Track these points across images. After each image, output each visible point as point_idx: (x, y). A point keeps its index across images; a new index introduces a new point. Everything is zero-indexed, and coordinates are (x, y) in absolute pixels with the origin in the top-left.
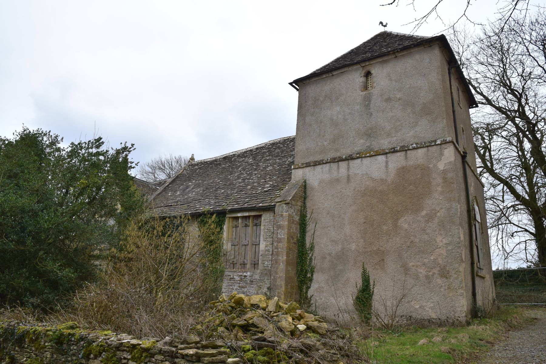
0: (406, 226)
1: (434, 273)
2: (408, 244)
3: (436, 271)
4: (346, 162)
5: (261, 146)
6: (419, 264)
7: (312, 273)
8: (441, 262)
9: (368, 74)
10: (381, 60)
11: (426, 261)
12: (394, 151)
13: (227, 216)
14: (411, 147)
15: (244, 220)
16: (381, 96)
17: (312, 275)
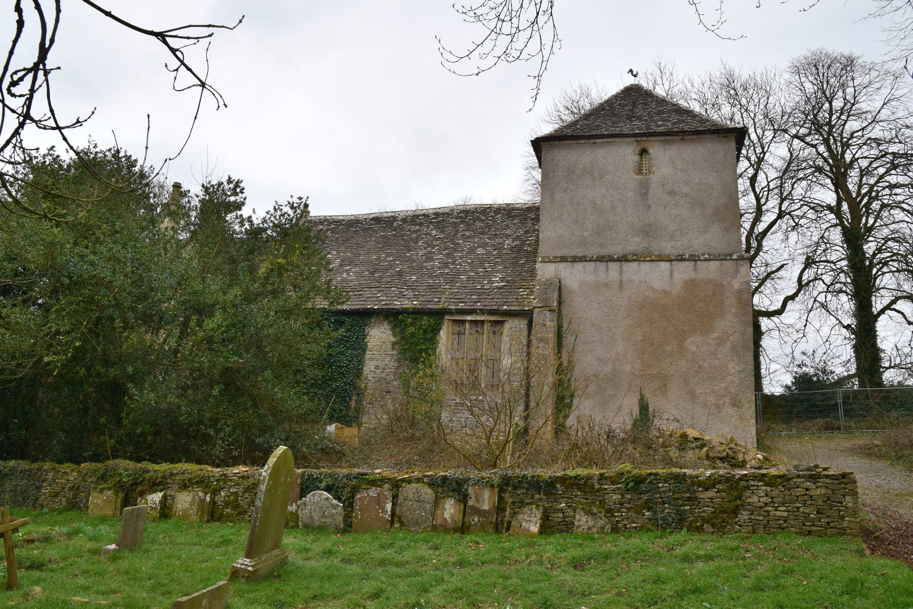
0: (694, 348)
1: (725, 402)
2: (696, 369)
3: (727, 399)
4: (619, 263)
5: (442, 210)
6: (709, 391)
7: (572, 396)
9: (643, 152)
10: (663, 138)
11: (716, 388)
12: (680, 258)
13: (446, 317)
14: (702, 258)
16: (663, 186)
17: (572, 401)
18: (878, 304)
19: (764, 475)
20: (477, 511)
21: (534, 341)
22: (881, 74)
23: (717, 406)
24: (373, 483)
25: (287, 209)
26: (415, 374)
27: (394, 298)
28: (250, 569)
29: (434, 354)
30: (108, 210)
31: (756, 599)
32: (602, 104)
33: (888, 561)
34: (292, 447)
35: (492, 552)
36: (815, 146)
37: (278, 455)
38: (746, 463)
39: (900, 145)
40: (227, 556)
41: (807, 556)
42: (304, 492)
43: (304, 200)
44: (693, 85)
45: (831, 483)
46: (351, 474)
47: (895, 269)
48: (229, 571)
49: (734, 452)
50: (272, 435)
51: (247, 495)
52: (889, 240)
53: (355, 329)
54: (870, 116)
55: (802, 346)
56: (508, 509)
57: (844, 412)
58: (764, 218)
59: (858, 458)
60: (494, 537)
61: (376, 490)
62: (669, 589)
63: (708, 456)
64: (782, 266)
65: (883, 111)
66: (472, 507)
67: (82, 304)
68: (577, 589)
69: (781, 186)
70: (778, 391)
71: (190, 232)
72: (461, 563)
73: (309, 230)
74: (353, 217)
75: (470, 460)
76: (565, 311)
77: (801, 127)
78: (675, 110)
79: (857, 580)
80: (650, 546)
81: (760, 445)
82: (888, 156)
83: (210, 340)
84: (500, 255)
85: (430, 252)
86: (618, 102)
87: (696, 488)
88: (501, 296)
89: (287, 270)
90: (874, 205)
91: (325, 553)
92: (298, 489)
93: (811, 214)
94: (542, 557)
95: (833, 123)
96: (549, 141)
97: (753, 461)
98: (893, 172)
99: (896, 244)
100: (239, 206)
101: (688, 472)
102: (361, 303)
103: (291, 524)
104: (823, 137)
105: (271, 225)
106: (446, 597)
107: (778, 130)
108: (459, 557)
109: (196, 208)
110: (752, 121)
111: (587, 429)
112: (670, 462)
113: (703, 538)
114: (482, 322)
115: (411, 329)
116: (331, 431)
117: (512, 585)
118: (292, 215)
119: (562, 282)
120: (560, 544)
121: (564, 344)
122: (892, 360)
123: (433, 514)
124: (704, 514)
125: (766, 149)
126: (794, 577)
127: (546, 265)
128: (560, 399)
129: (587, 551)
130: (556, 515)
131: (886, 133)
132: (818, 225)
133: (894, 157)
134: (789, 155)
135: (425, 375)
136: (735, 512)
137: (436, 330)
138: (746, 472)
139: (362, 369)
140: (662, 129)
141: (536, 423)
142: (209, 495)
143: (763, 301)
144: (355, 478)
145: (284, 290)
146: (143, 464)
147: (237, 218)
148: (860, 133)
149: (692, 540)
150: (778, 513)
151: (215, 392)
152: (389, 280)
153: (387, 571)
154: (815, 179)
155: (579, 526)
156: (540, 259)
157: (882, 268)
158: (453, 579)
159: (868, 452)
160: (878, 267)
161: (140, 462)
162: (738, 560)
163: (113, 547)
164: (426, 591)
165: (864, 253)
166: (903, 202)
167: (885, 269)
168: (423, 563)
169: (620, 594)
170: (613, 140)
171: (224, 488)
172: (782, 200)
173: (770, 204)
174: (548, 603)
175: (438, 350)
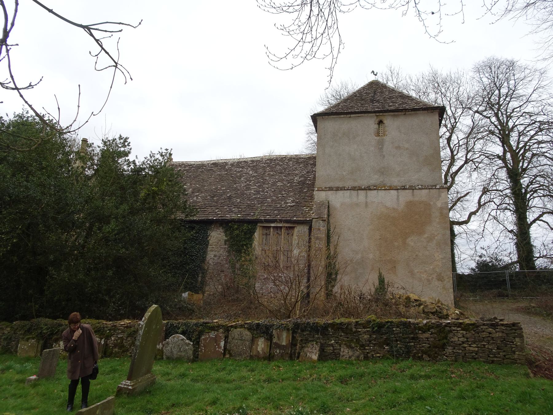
0: (412, 244)
1: (433, 278)
2: (414, 257)
3: (434, 276)
4: (365, 191)
7: (336, 274)
8: (438, 270)
9: (380, 122)
12: (404, 188)
13: (258, 225)
14: (417, 188)
15: (287, 230)
16: (392, 143)
17: (336, 277)
18: (530, 217)
19: (461, 323)
20: (278, 346)
21: (313, 239)
22: (532, 71)
23: (428, 280)
24: (213, 329)
25: (158, 156)
26: (239, 260)
27: (226, 213)
28: (130, 387)
29: (251, 247)
30: (37, 154)
31: (460, 404)
32: (355, 93)
33: (546, 381)
34: (161, 306)
35: (288, 373)
36: (489, 118)
37: (151, 311)
38: (449, 316)
39: (544, 116)
40: (114, 380)
41: (492, 377)
42: (167, 336)
43: (169, 151)
44: (411, 81)
45: (506, 329)
46: (199, 323)
47: (542, 195)
48: (115, 390)
49: (441, 309)
50: (147, 300)
51: (129, 339)
52: (537, 176)
53: (201, 232)
54: (525, 98)
55: (482, 243)
56: (298, 344)
57: (511, 285)
58: (456, 164)
59: (522, 315)
60: (289, 363)
61: (214, 333)
62: (403, 397)
63: (424, 311)
64: (468, 193)
65: (533, 95)
66: (276, 343)
67: (18, 214)
68: (344, 396)
69: (467, 143)
70: (467, 272)
71: (94, 170)
72: (269, 380)
73: (172, 169)
74: (200, 163)
75: (274, 314)
76: (331, 221)
77: (480, 106)
78: (400, 96)
79: (526, 392)
80: (389, 368)
81: (457, 305)
82: (536, 123)
83: (107, 240)
84: (291, 187)
85: (249, 185)
86: (365, 92)
87: (417, 331)
88: (292, 212)
89: (158, 195)
90: (527, 154)
91: (180, 376)
92: (163, 334)
93: (486, 161)
94: (320, 375)
95: (501, 103)
96: (322, 116)
97: (453, 315)
98: (540, 133)
99: (542, 179)
100: (126, 154)
101: (412, 320)
102: (205, 216)
103: (158, 357)
104: (494, 112)
105: (148, 166)
106: (259, 403)
107: (465, 108)
108: (267, 376)
109: (98, 154)
110: (448, 103)
111: (347, 292)
112: (400, 315)
113: (423, 364)
114: (281, 227)
115: (237, 232)
116: (185, 296)
117: (302, 394)
118: (162, 160)
119: (330, 203)
120: (331, 367)
121: (331, 241)
122: (541, 252)
123: (251, 348)
124: (423, 348)
125: (457, 121)
126: (485, 390)
127: (320, 192)
128: (329, 275)
129: (349, 372)
130: (329, 348)
131: (535, 109)
132: (490, 168)
133: (541, 124)
134: (472, 124)
135: (246, 260)
136: (443, 347)
137: (252, 232)
138: (449, 321)
139: (206, 257)
140: (392, 108)
141: (314, 290)
142: (103, 340)
143: (454, 215)
144: (201, 325)
145: (156, 207)
146: (58, 321)
147: (125, 161)
148: (518, 109)
149: (416, 365)
150: (471, 348)
151: (110, 273)
152: (223, 201)
153: (221, 386)
154: (488, 138)
155: (343, 356)
156: (316, 189)
157: (533, 194)
158: (264, 391)
159: (527, 311)
160: (530, 193)
161: (55, 319)
162: (447, 378)
163: (34, 377)
164: (246, 399)
165: (521, 185)
166: (546, 152)
167: (535, 195)
168: (244, 380)
169: (371, 400)
170: (362, 115)
171: (114, 334)
172: (468, 152)
173: (460, 155)
174: (325, 406)
175: (253, 245)
